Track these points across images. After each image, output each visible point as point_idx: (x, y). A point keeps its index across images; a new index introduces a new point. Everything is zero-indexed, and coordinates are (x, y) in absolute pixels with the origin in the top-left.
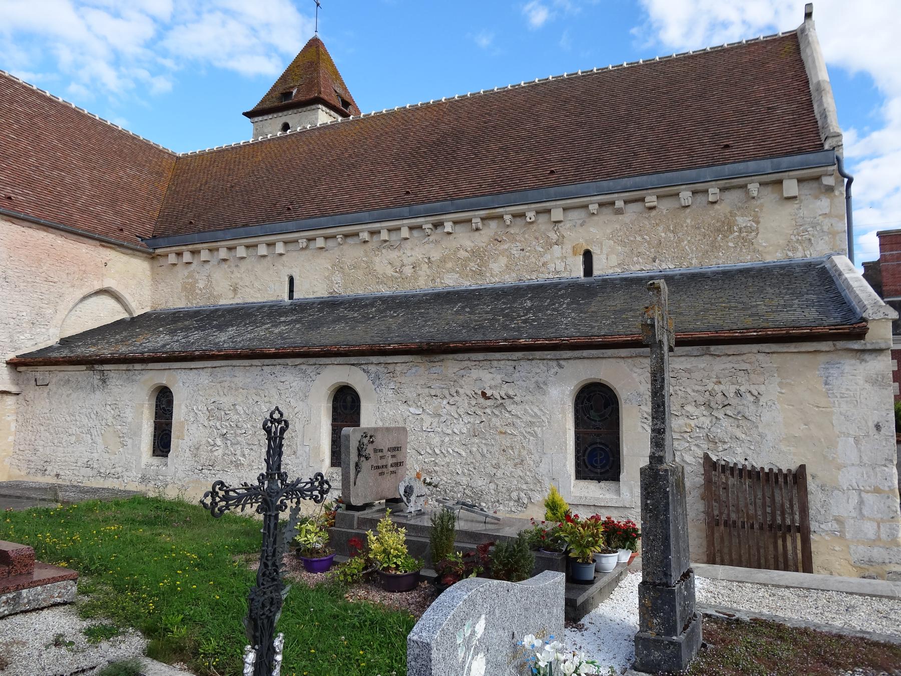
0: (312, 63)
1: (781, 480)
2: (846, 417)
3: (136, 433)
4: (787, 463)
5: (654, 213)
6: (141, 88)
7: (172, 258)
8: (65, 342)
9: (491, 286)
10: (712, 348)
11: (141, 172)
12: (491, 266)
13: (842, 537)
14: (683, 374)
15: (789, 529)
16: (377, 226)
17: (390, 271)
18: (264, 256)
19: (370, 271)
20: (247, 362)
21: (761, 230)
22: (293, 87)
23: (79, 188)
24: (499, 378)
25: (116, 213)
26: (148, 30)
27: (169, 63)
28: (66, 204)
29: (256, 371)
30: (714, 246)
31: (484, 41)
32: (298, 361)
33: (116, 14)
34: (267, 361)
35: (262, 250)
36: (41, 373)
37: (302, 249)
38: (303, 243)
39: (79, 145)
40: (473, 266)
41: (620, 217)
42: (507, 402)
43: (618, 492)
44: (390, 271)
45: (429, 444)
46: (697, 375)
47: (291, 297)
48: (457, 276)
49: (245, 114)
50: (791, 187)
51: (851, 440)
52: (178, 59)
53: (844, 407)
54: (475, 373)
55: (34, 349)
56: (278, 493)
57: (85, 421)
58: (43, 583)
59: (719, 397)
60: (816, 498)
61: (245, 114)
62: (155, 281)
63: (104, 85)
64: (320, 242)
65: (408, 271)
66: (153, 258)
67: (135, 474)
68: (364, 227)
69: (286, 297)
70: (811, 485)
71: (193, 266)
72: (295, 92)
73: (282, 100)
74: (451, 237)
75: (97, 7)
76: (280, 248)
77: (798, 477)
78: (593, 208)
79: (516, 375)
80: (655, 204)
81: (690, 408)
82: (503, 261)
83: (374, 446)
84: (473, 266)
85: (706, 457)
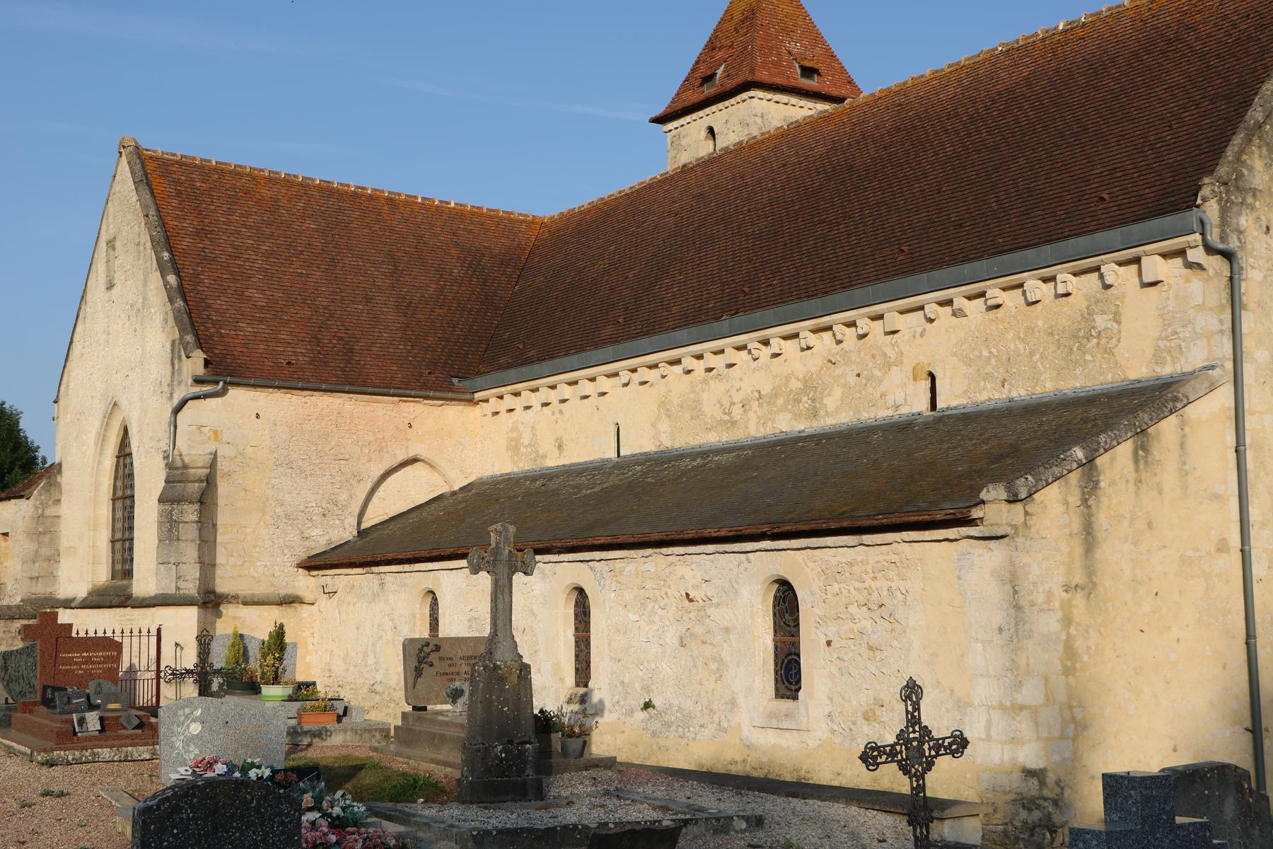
16: (502, 389)
44: (719, 415)
65: (737, 412)
72: (720, 72)
82: (838, 392)
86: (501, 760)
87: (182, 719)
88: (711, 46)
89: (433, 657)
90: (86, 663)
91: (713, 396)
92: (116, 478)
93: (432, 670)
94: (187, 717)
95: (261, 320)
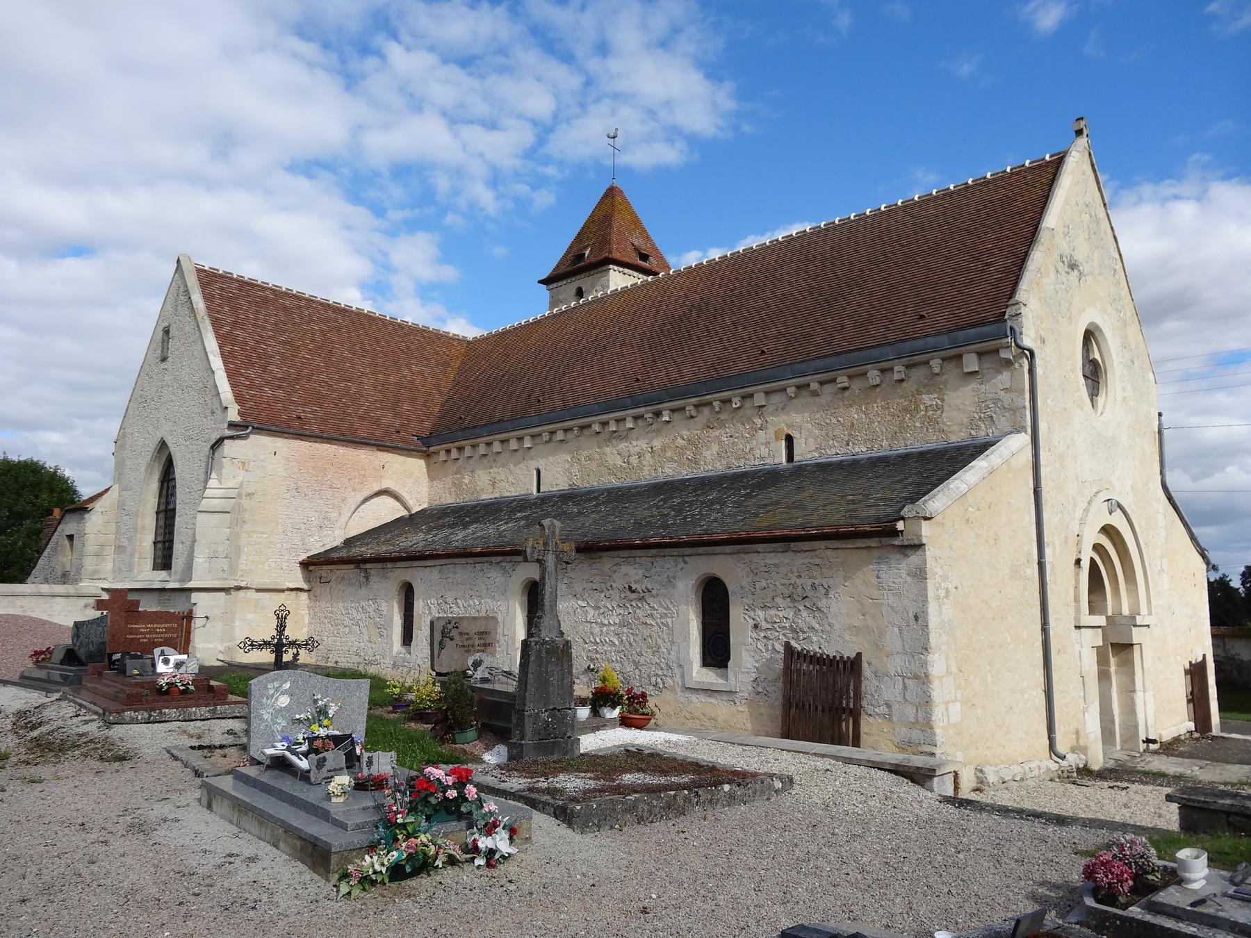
0: (606, 217)
1: (841, 666)
2: (892, 608)
3: (389, 625)
4: (849, 653)
5: (847, 393)
6: (522, 205)
7: (443, 456)
8: (349, 542)
9: (704, 474)
10: (792, 544)
11: (426, 366)
12: (705, 453)
13: (890, 720)
14: (773, 569)
15: (844, 710)
16: (605, 417)
17: (619, 462)
18: (516, 451)
19: (603, 463)
20: (463, 561)
21: (946, 408)
22: (586, 248)
23: (362, 396)
24: (641, 572)
25: (396, 415)
26: (527, 137)
27: (550, 171)
28: (349, 415)
29: (470, 568)
30: (902, 427)
31: (965, 69)
32: (499, 559)
33: (492, 125)
34: (477, 559)
35: (514, 445)
36: (324, 571)
37: (547, 442)
38: (546, 436)
39: (367, 351)
40: (689, 454)
41: (818, 399)
42: (647, 595)
43: (727, 679)
44: (619, 462)
45: (592, 633)
46: (783, 570)
47: (539, 491)
48: (675, 465)
49: (540, 282)
50: (971, 362)
51: (896, 630)
52: (561, 164)
53: (892, 600)
54: (625, 569)
55: (322, 550)
56: (284, 645)
57: (355, 614)
58: (230, 703)
59: (799, 590)
60: (869, 683)
61: (540, 282)
62: (432, 477)
63: (482, 210)
64: (560, 435)
65: (634, 460)
66: (427, 456)
67: (388, 662)
68: (594, 418)
69: (535, 492)
70: (867, 671)
71: (460, 462)
72: (587, 253)
73: (578, 266)
74: (670, 426)
75: (471, 122)
76: (527, 443)
77: (853, 666)
78: (791, 391)
79: (654, 570)
80: (846, 384)
81: (778, 600)
82: (715, 448)
83: (460, 630)
84: (689, 454)
85: (787, 646)
86: (547, 723)
87: (271, 692)
88: (579, 238)
89: (454, 633)
90: (150, 633)
91: (613, 454)
92: (160, 497)
93: (453, 643)
94: (277, 690)
95: (280, 387)
